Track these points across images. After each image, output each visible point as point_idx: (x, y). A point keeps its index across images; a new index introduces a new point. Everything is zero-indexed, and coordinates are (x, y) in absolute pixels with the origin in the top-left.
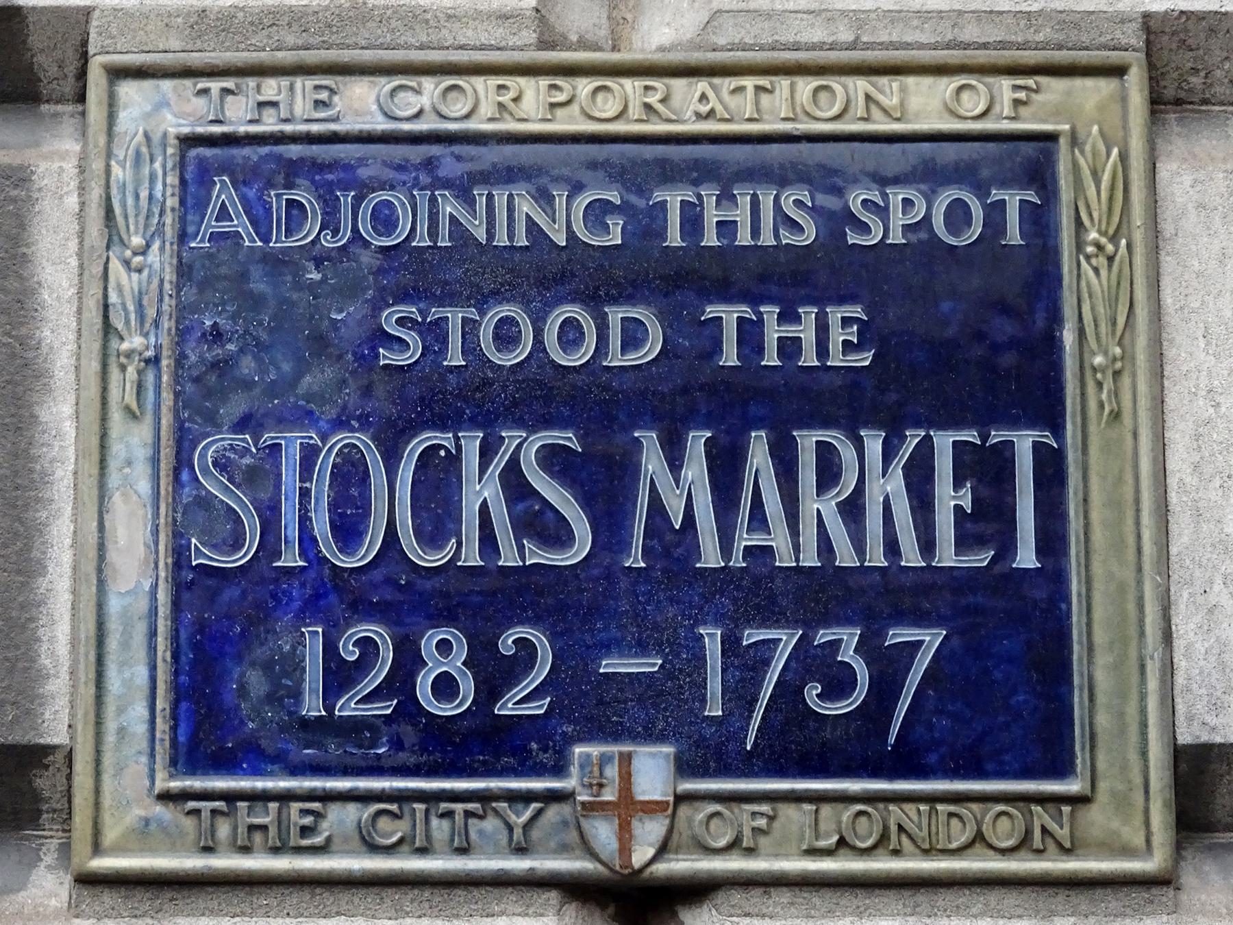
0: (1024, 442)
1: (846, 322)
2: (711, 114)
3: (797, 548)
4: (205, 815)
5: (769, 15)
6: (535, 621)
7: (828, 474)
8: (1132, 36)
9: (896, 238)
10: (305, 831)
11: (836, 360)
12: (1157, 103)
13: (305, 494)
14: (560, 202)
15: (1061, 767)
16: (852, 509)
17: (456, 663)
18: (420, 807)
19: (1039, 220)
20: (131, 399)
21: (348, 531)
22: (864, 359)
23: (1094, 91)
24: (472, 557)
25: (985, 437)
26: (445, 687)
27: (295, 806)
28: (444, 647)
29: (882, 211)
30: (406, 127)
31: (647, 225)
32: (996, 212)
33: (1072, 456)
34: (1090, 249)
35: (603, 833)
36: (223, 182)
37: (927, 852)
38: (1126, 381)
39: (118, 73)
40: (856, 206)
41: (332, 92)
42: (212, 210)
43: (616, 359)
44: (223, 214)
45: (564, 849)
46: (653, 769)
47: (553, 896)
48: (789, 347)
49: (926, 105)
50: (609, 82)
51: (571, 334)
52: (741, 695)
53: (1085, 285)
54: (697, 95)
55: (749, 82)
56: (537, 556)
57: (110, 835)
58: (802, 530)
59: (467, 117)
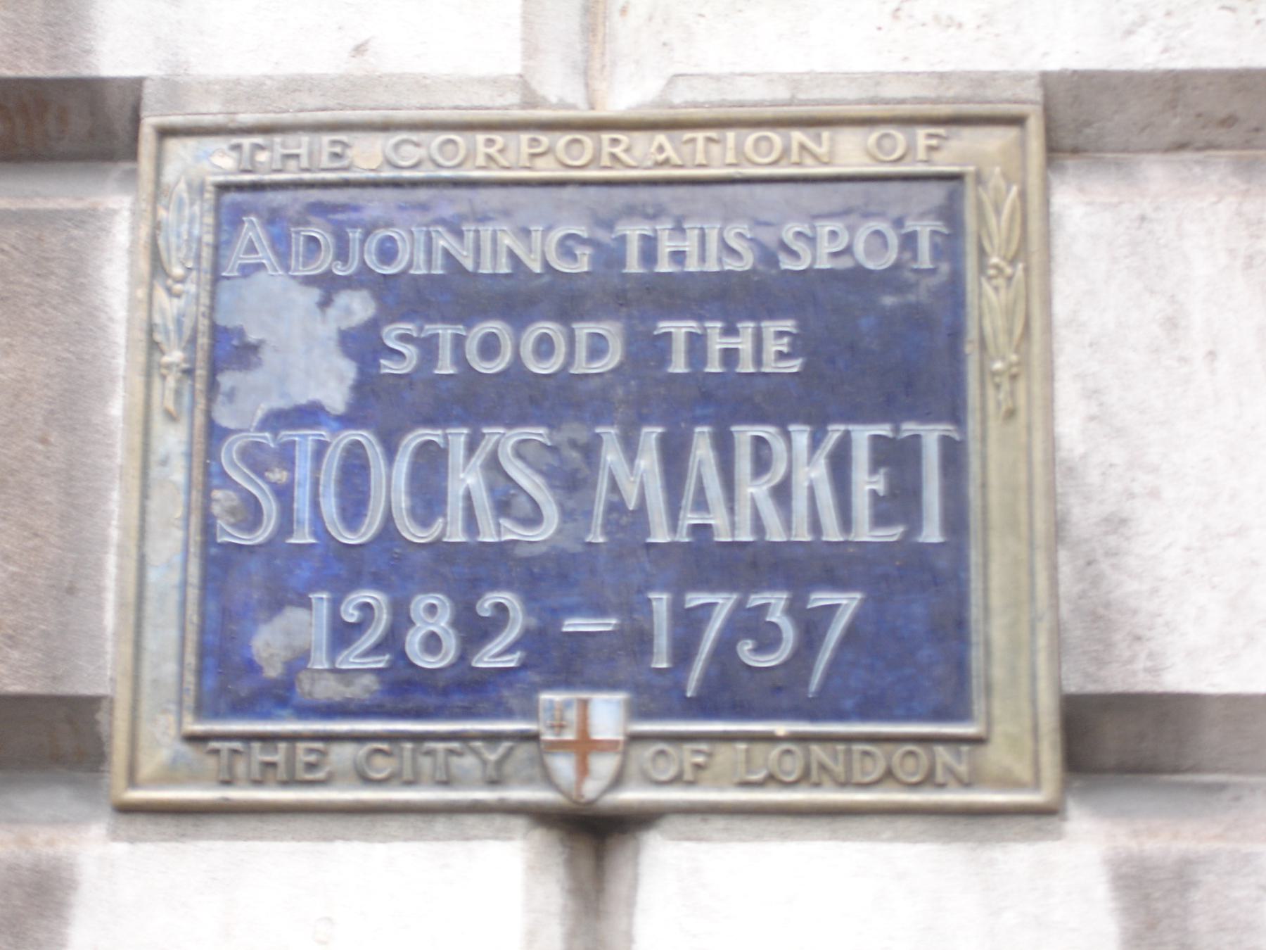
0: (931, 436)
1: (780, 334)
2: (666, 163)
3: (733, 526)
4: (224, 754)
5: (717, 78)
6: (509, 586)
7: (761, 464)
8: (1033, 92)
9: (824, 264)
10: (311, 767)
11: (771, 366)
12: (1053, 150)
13: (316, 483)
14: (536, 237)
15: (956, 709)
16: (782, 493)
17: (441, 624)
18: (408, 746)
19: (950, 245)
20: (170, 405)
21: (353, 511)
22: (794, 366)
23: (993, 141)
24: (457, 535)
25: (897, 430)
26: (432, 643)
27: (301, 746)
28: (432, 609)
29: (811, 240)
30: (407, 174)
31: (610, 257)
32: (909, 241)
33: (974, 447)
34: (992, 272)
35: (563, 766)
36: (252, 222)
37: (844, 784)
38: (1021, 385)
39: (165, 133)
40: (788, 237)
41: (345, 145)
42: (241, 244)
43: (581, 366)
44: (251, 249)
45: (528, 782)
46: (607, 714)
47: (519, 823)
48: (730, 356)
49: (851, 152)
50: (578, 136)
51: (544, 347)
52: (683, 652)
53: (989, 304)
54: (656, 144)
55: (700, 135)
56: (513, 532)
57: (147, 768)
58: (741, 511)
59: (459, 166)
